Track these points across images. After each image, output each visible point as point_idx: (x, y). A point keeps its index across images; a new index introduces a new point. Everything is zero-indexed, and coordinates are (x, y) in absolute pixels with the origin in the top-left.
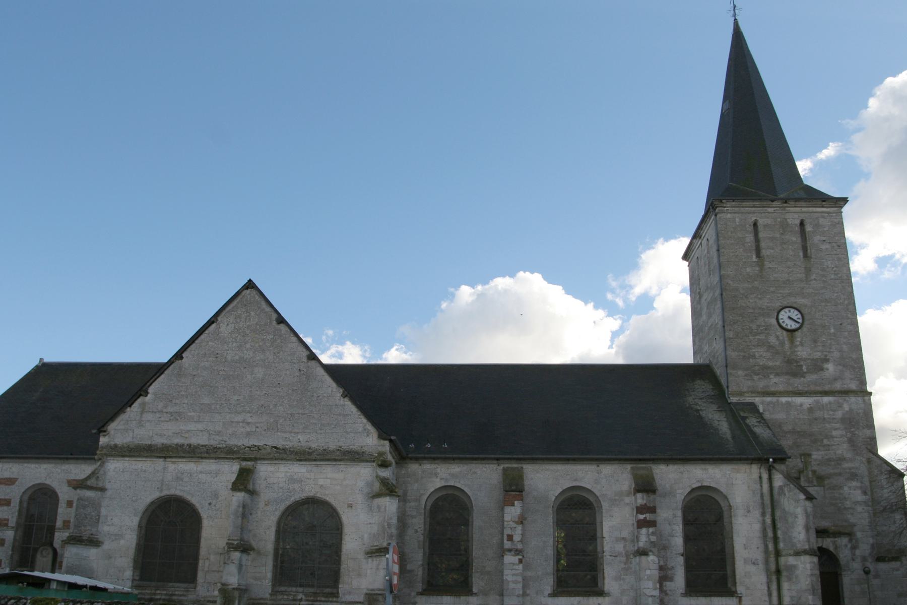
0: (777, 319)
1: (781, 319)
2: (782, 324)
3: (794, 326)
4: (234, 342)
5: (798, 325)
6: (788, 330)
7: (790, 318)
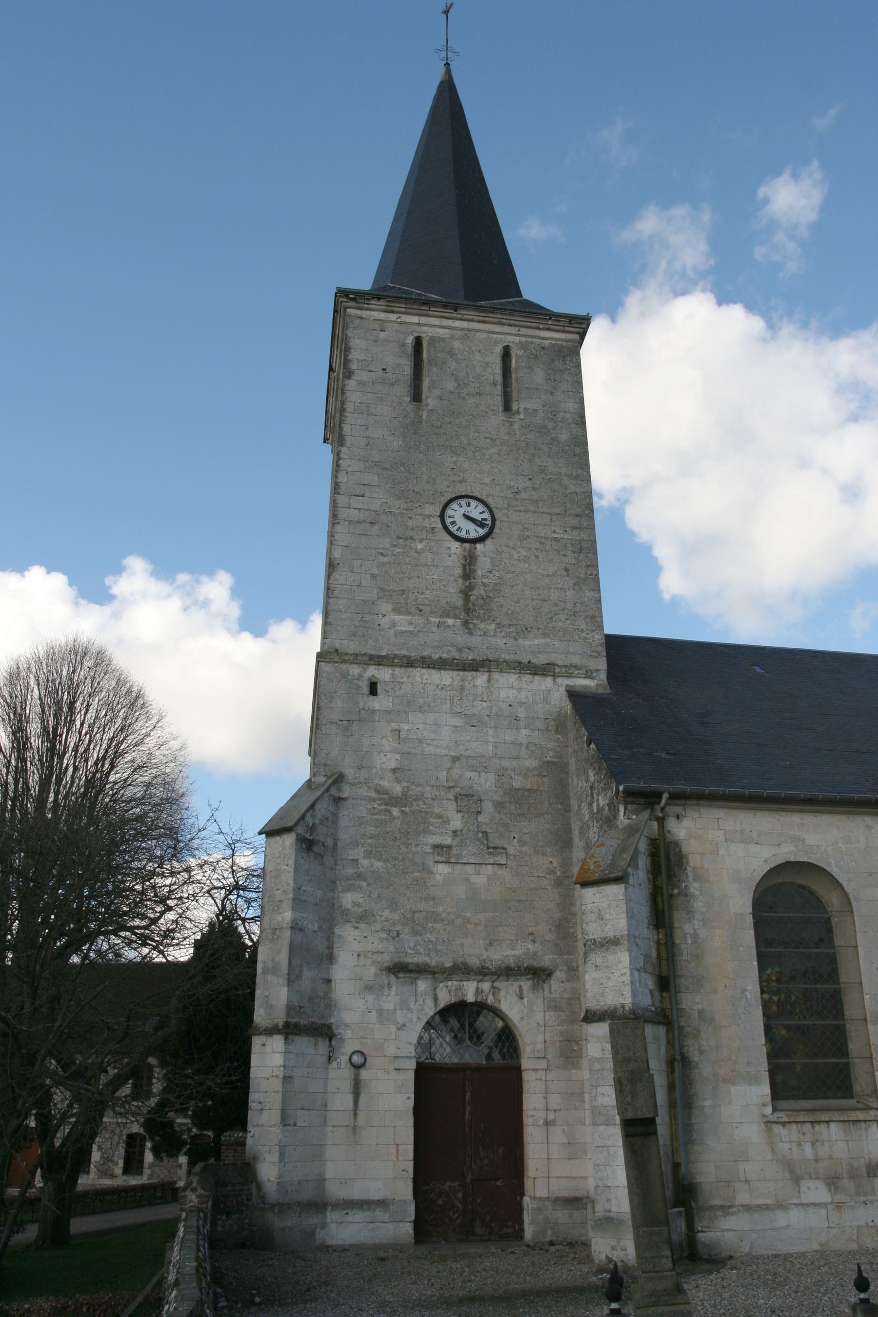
0: (442, 516)
1: (450, 517)
2: (458, 534)
3: (475, 532)
4: (124, 864)
5: (482, 532)
6: (462, 540)
7: (467, 517)
